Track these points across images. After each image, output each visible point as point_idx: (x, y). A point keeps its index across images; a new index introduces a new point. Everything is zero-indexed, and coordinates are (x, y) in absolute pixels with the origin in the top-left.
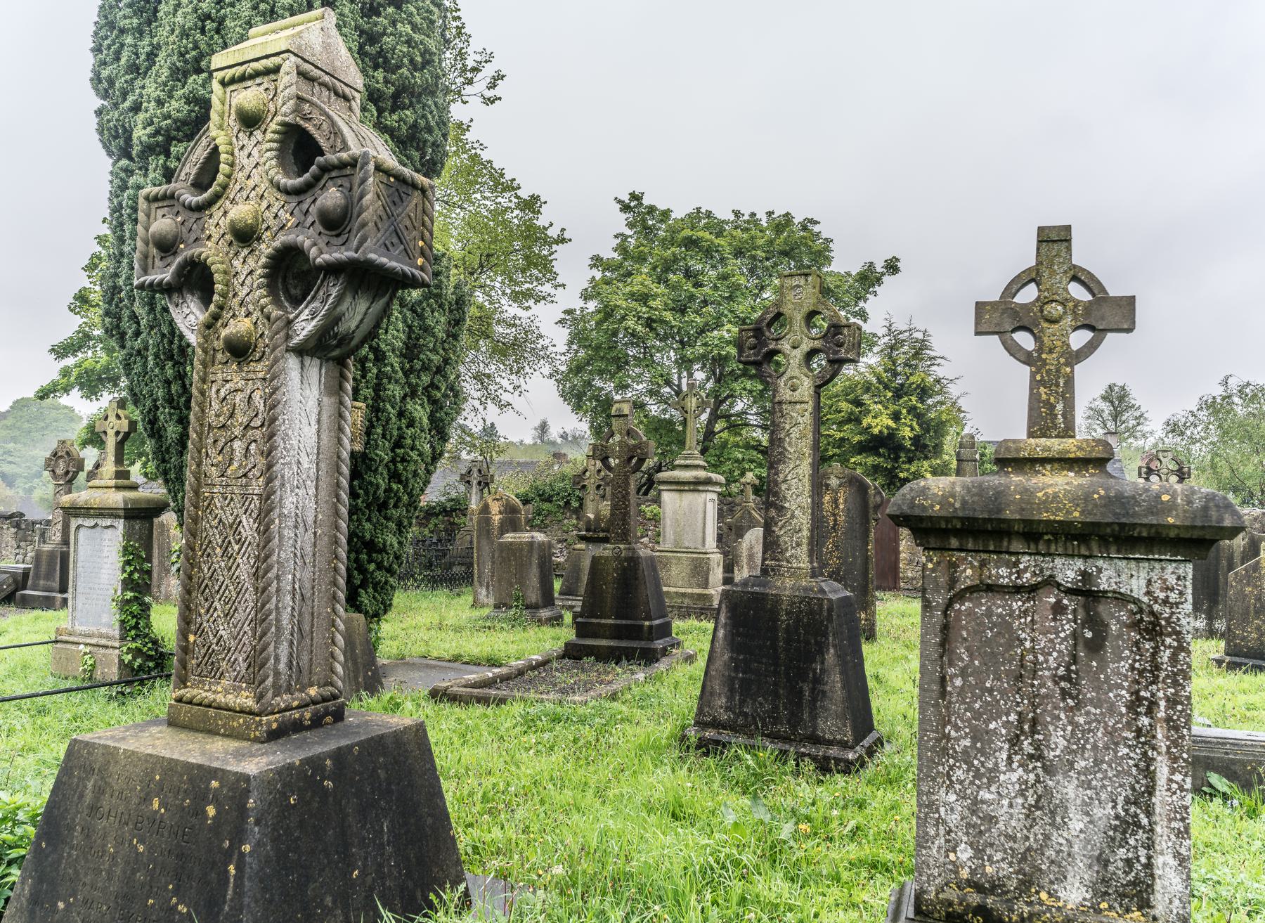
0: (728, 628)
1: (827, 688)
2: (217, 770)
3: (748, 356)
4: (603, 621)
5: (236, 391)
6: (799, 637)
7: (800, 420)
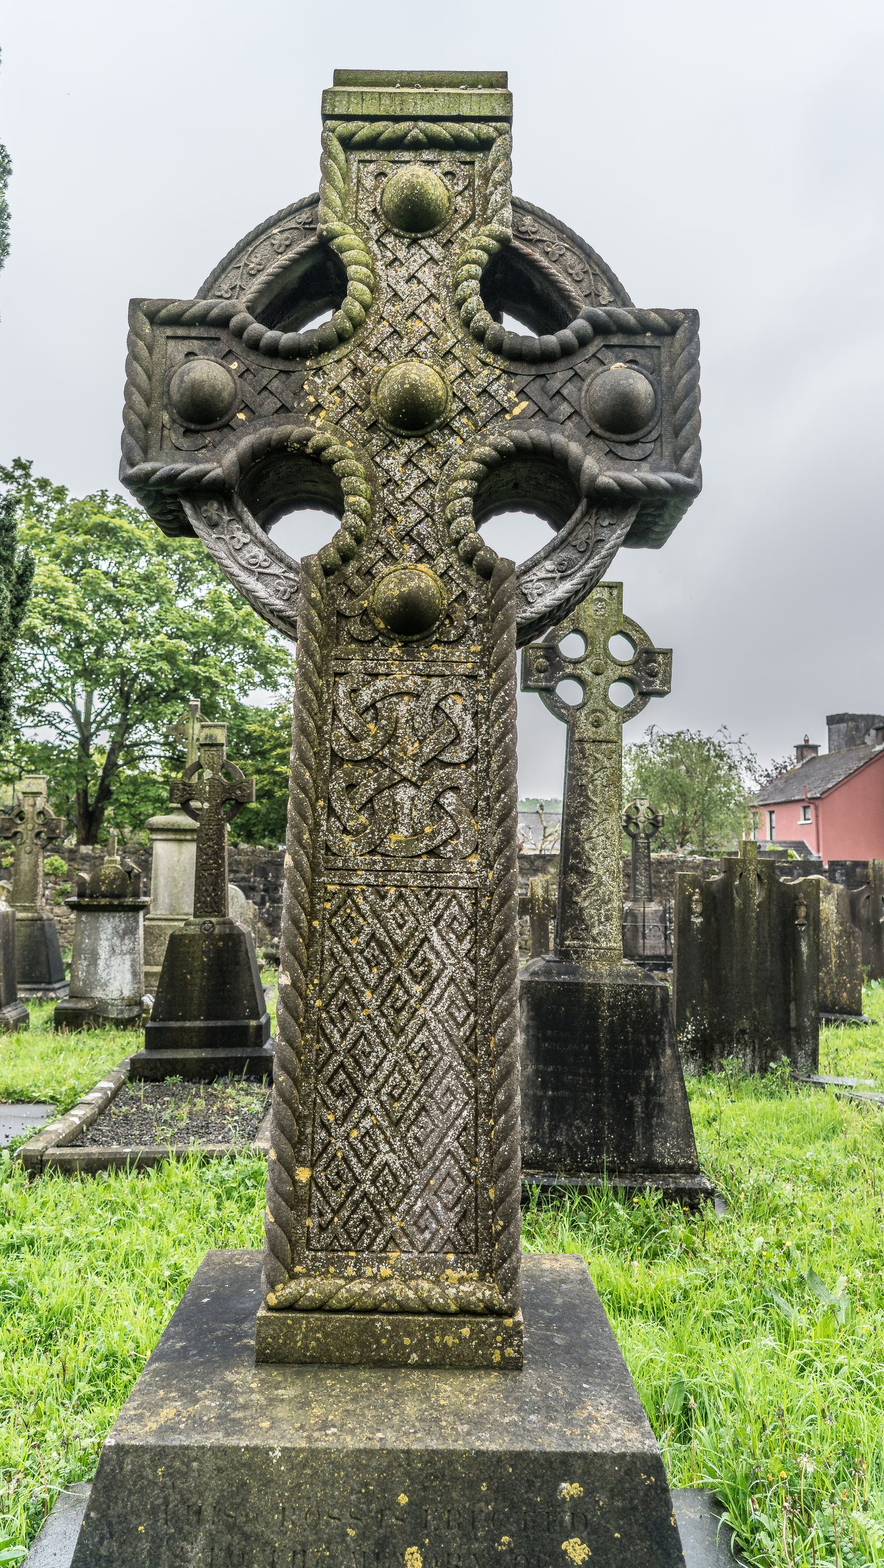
0: (531, 1032)
1: (664, 1099)
2: (565, 1458)
3: (537, 681)
4: (188, 1024)
5: (400, 694)
6: (626, 1037)
7: (606, 763)
